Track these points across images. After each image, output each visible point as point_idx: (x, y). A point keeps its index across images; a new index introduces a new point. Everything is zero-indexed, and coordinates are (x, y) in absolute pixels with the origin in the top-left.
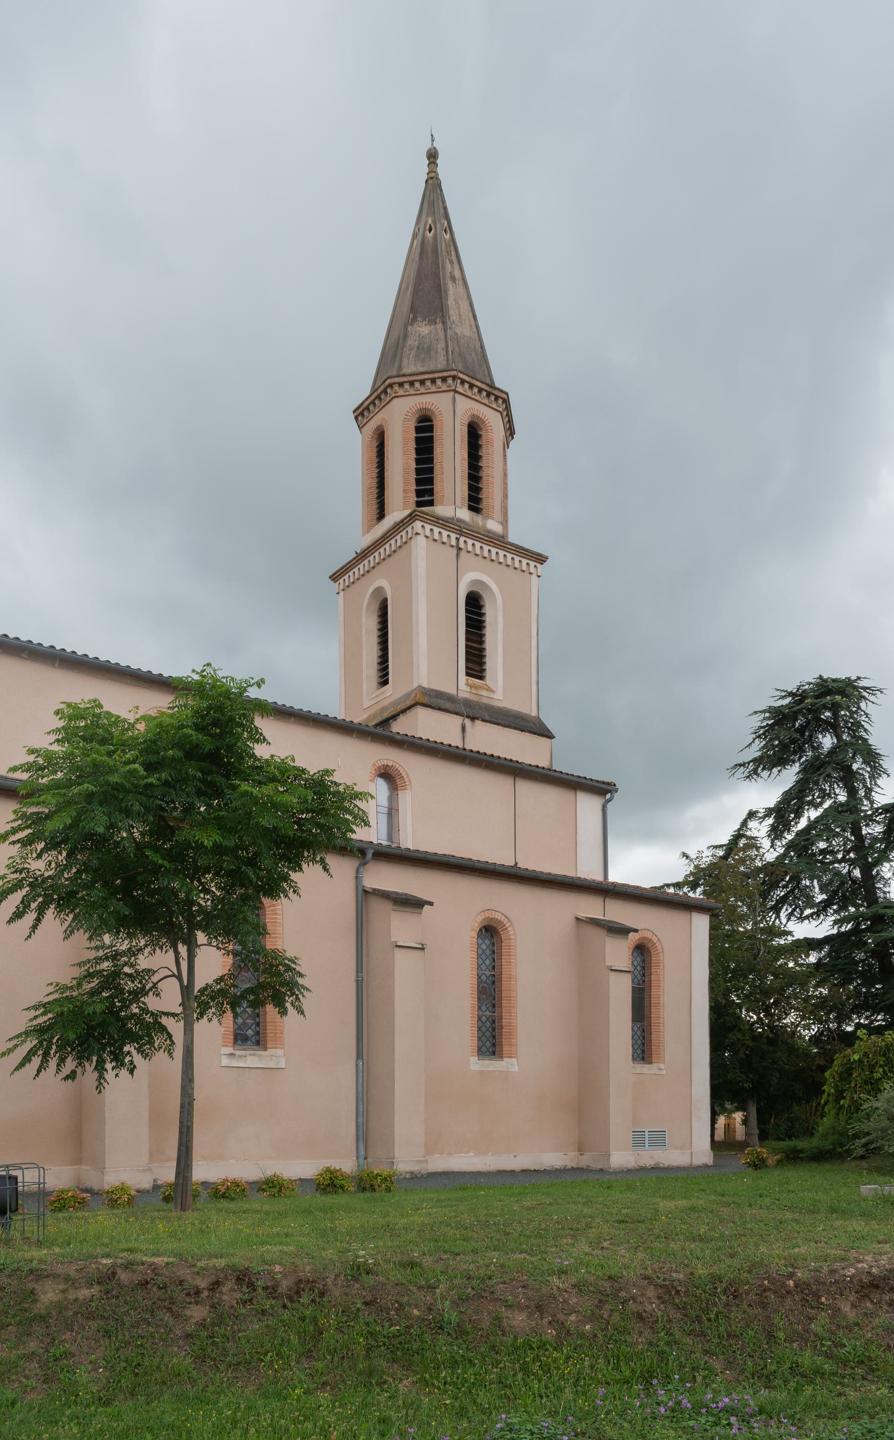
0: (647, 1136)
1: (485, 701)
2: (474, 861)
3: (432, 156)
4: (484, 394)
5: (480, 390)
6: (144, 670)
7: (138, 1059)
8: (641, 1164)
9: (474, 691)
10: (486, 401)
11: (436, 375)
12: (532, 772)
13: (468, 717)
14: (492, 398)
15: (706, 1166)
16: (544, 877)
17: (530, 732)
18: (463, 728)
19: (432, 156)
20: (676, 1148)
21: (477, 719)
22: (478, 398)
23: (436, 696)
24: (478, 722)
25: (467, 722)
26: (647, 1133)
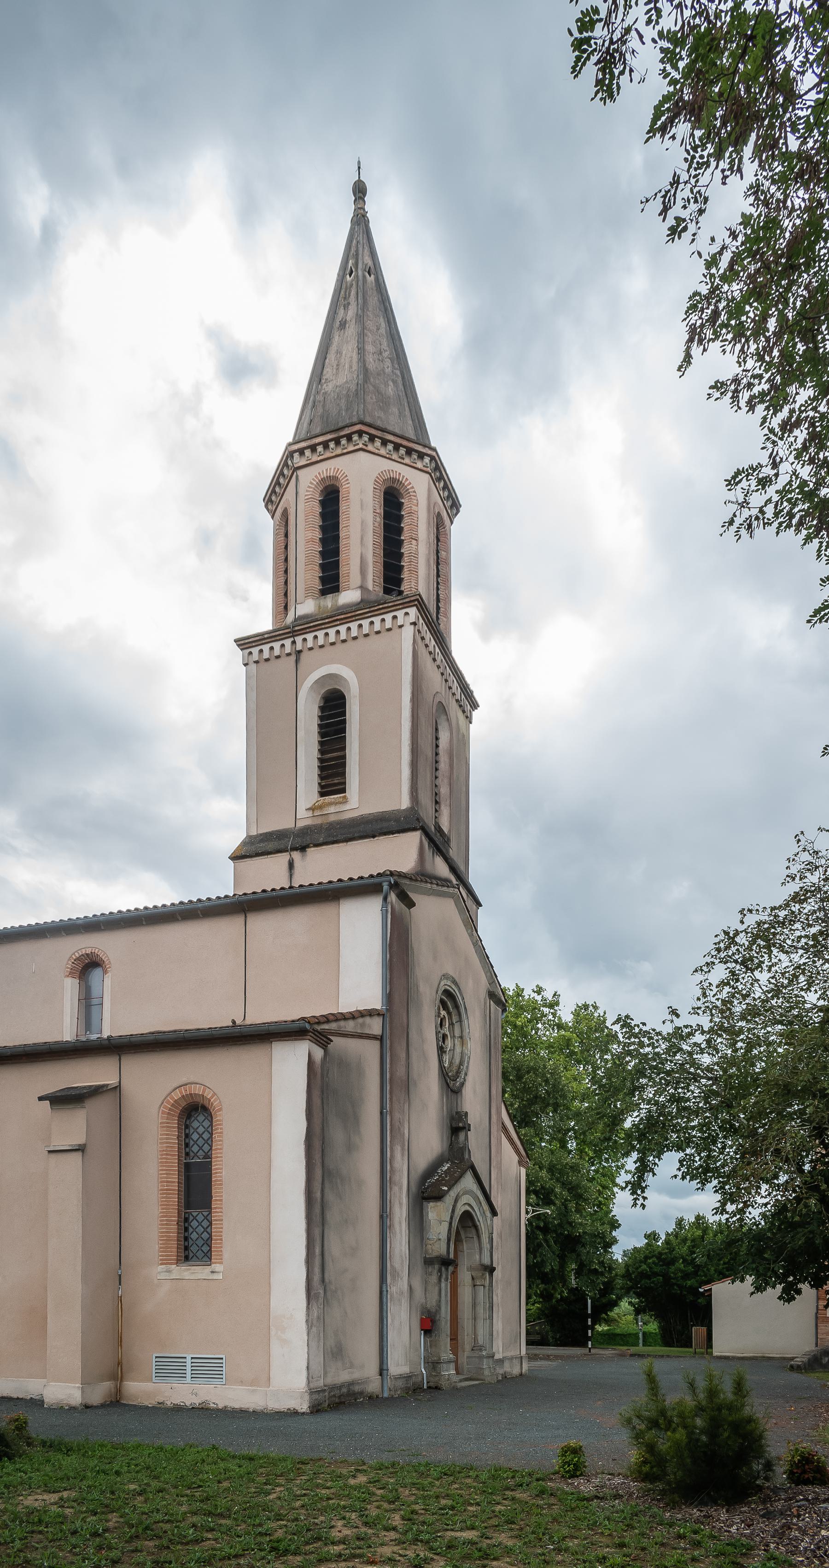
0: (189, 1365)
1: (332, 818)
2: (10, 1048)
3: (360, 191)
4: (332, 445)
5: (325, 445)
6: (50, 921)
7: (612, 1214)
8: (658, 1379)
9: (317, 813)
10: (339, 451)
11: (405, 443)
12: (326, 891)
13: (294, 849)
14: (344, 441)
15: (295, 1413)
16: (9, 1052)
17: (385, 834)
18: (291, 865)
19: (360, 191)
20: (242, 1383)
21: (308, 846)
22: (328, 454)
23: (262, 841)
24: (311, 851)
25: (296, 855)
26: (189, 1360)
